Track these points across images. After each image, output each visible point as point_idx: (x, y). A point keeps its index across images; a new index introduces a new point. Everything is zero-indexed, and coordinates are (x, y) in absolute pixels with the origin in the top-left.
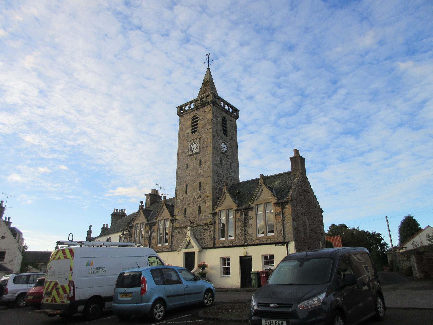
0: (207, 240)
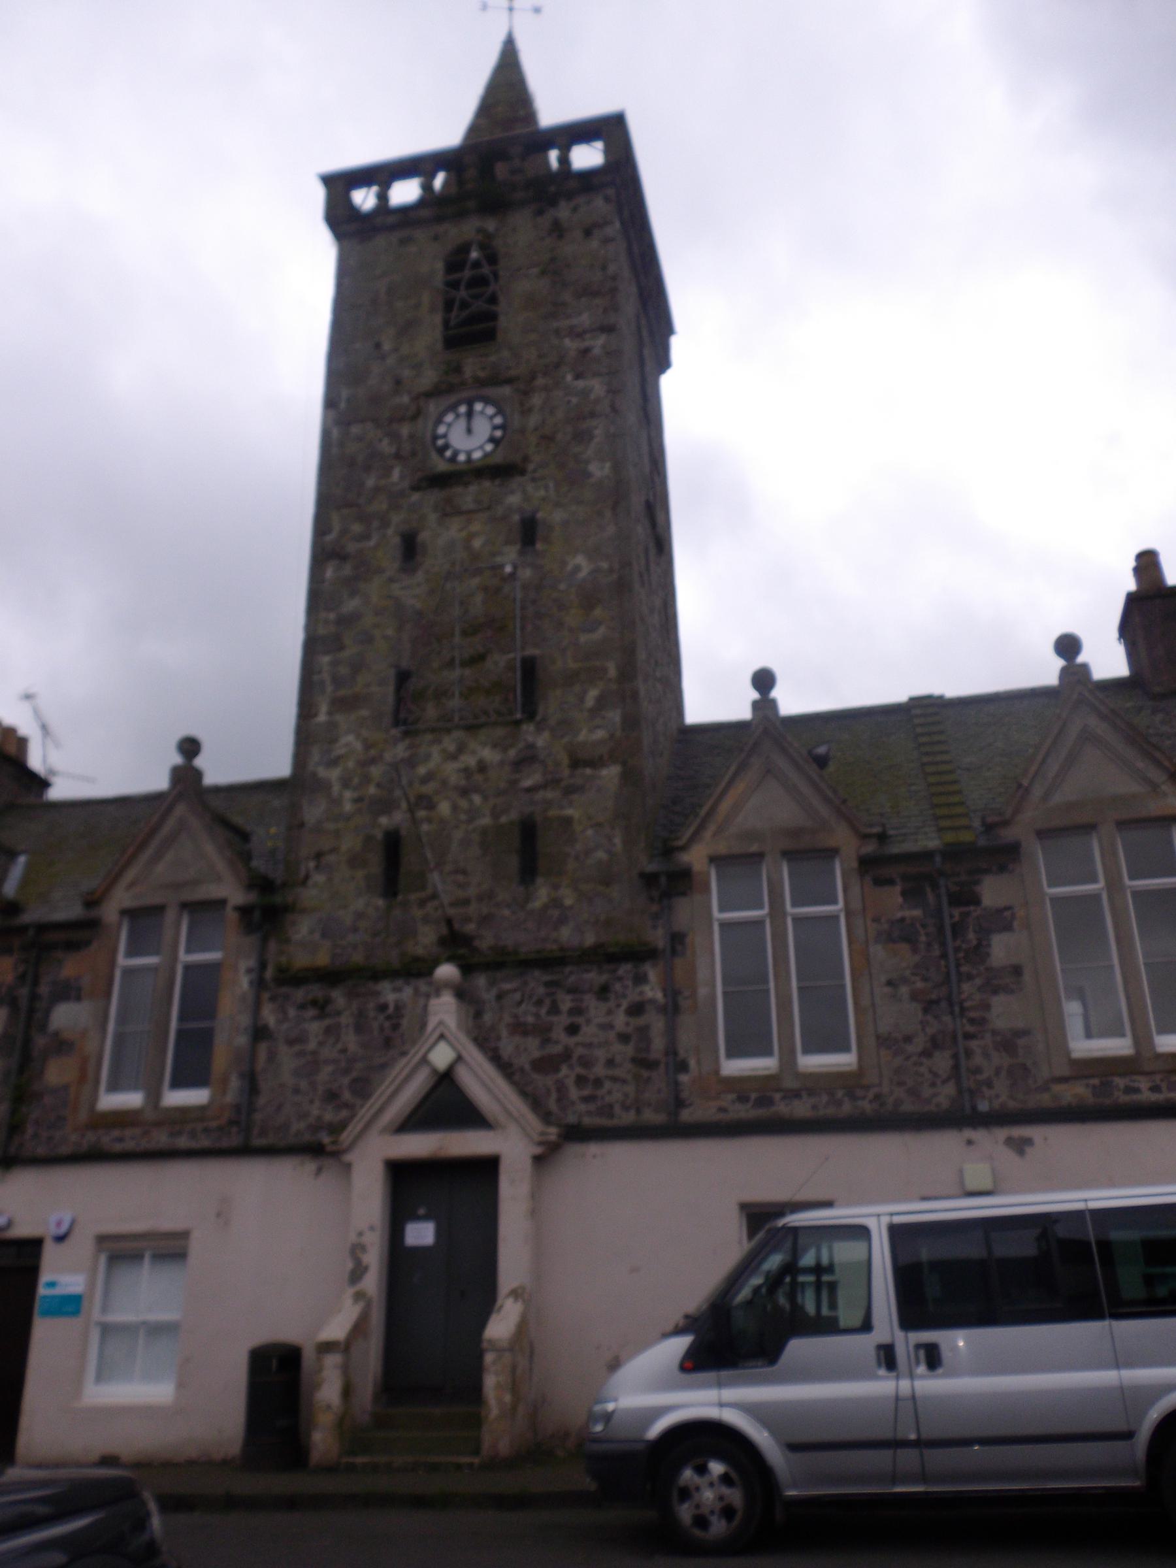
0: (599, 1070)
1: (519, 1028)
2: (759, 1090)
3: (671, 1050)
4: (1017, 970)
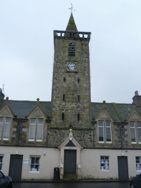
0: (86, 141)
1: (78, 136)
2: (103, 145)
3: (94, 140)
4: (127, 135)
